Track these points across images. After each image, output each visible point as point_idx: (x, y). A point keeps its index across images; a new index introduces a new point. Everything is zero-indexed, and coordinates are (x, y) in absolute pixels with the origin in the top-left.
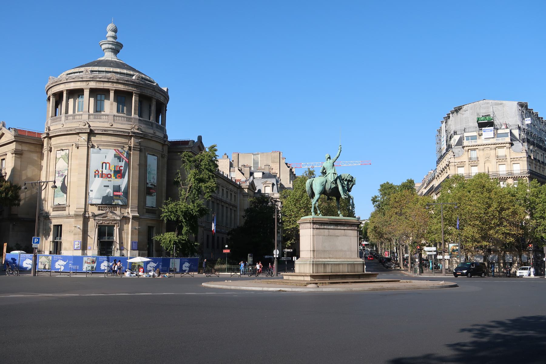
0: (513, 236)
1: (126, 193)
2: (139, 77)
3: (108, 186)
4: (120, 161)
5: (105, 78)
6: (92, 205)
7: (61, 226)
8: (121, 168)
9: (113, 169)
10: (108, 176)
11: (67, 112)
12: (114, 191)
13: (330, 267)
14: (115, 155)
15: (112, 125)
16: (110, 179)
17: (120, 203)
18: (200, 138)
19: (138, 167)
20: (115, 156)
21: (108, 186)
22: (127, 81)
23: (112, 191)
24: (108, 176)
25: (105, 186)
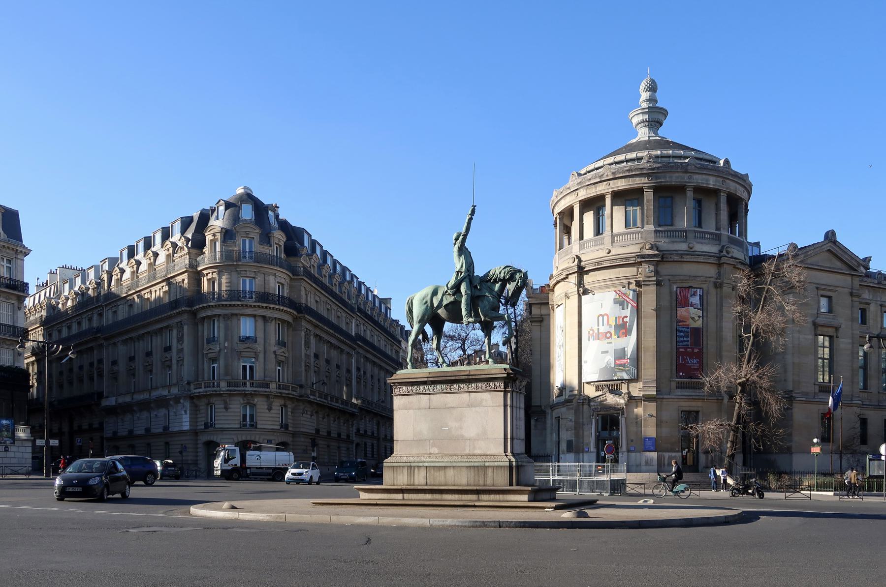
0: (787, 413)
1: (637, 359)
2: (650, 157)
3: (607, 352)
4: (623, 309)
5: (595, 178)
6: (589, 383)
7: (697, 412)
8: (625, 320)
10: (607, 336)
11: (581, 237)
12: (616, 358)
15: (609, 252)
16: (609, 340)
17: (626, 377)
20: (616, 301)
22: (628, 171)
23: (612, 360)
25: (603, 352)
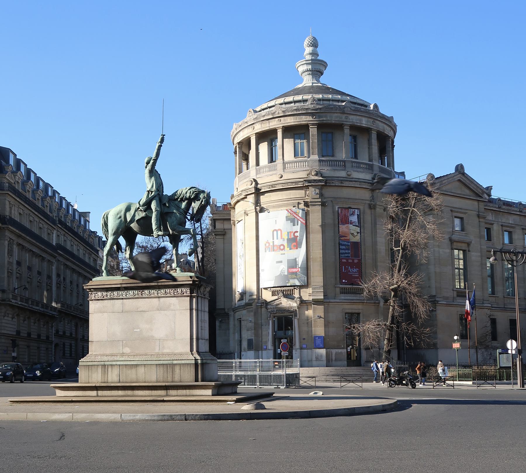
3: (281, 262)
4: (294, 225)
6: (266, 289)
8: (296, 234)
9: (286, 238)
10: (281, 248)
13: (116, 371)
14: (287, 217)
15: (281, 177)
16: (283, 252)
17: (298, 283)
18: (460, 169)
19: (320, 229)
20: (288, 219)
21: (281, 262)
22: (296, 110)
23: (286, 268)
24: (281, 248)
